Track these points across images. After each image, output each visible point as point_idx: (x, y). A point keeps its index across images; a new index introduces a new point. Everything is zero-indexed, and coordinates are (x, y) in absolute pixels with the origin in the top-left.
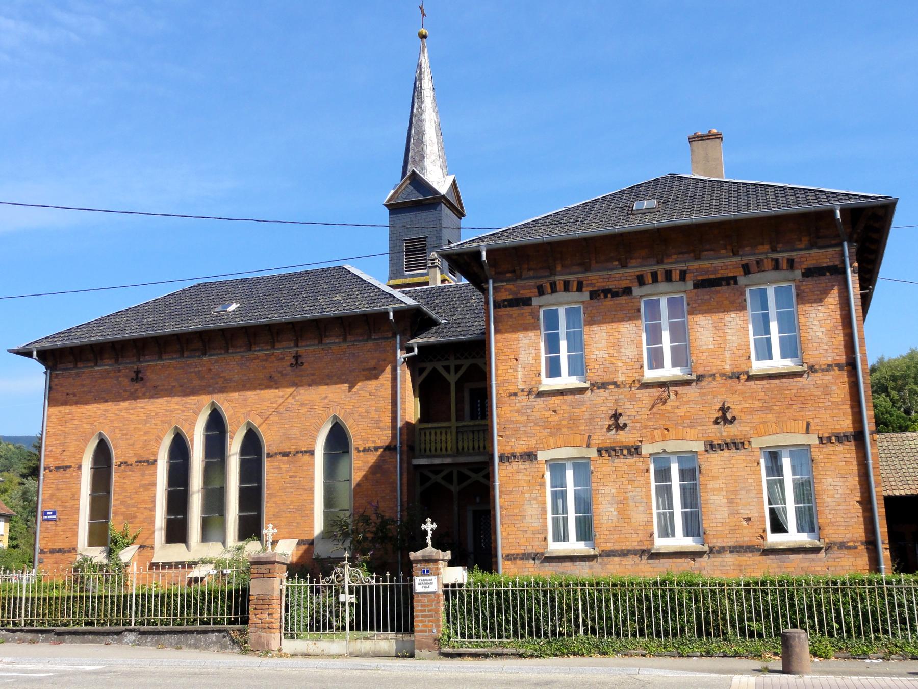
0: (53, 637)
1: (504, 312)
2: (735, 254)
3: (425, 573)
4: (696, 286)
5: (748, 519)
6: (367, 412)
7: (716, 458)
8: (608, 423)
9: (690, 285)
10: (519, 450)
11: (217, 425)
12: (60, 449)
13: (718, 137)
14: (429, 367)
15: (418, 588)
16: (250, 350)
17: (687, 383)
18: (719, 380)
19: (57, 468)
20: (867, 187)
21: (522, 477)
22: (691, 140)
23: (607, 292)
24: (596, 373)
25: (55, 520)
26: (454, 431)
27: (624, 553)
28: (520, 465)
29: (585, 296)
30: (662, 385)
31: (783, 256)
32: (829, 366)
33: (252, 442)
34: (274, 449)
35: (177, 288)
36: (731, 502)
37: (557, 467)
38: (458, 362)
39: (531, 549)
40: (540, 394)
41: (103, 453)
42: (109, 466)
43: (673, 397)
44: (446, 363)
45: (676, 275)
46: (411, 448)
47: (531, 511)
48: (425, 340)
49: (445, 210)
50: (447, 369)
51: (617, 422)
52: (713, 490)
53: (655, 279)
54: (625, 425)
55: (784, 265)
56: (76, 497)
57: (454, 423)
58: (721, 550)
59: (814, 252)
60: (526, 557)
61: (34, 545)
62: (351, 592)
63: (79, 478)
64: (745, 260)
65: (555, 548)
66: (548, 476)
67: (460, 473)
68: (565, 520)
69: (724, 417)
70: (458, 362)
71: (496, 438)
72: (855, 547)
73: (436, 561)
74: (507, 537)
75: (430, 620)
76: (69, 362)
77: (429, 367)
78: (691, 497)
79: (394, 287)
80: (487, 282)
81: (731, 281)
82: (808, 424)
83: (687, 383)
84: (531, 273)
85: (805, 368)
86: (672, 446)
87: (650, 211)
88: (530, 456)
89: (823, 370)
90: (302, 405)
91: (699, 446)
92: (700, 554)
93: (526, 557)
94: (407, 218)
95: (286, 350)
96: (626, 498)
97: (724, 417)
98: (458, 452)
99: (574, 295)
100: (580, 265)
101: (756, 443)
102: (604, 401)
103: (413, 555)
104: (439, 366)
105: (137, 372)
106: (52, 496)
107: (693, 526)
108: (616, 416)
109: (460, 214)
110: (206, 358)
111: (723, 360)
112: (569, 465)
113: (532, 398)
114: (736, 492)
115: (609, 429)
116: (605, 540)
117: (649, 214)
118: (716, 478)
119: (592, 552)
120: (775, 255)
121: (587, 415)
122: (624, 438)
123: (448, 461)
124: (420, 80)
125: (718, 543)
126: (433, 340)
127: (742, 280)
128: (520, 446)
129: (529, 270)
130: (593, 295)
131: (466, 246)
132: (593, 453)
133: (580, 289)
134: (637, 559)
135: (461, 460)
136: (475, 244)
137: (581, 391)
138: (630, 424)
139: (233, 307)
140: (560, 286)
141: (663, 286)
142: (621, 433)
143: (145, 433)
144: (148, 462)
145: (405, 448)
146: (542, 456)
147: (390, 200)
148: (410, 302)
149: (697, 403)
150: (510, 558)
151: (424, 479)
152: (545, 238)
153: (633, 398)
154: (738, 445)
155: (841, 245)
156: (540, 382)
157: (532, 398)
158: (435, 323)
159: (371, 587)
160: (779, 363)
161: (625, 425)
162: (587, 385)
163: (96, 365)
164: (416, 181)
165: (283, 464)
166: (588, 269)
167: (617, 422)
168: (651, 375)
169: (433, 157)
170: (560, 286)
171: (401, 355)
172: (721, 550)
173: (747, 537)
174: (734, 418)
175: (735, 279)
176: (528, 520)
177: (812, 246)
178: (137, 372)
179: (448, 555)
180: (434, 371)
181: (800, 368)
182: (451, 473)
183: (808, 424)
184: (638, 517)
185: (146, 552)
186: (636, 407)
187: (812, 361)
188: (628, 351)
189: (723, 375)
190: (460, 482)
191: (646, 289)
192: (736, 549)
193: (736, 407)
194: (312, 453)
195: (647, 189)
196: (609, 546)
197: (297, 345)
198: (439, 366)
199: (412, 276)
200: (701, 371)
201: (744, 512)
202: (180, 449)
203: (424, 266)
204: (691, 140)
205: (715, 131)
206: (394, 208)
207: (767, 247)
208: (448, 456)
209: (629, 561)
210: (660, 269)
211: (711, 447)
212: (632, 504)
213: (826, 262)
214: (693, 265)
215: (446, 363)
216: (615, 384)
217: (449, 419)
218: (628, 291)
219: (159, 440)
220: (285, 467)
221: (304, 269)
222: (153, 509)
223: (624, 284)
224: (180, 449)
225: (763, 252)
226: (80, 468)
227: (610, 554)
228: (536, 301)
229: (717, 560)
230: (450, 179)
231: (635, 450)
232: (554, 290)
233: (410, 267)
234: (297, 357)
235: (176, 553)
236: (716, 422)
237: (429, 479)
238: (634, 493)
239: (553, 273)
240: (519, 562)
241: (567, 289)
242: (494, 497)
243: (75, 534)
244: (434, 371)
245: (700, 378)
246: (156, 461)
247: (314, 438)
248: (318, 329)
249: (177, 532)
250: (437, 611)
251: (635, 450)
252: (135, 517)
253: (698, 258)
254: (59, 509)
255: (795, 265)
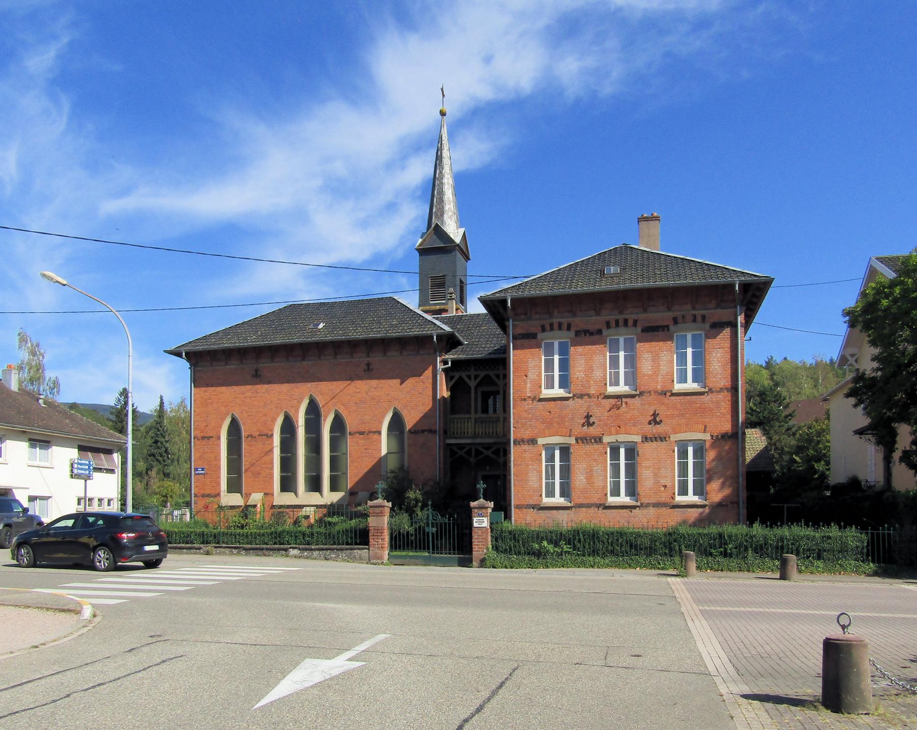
0: (243, 552)
1: (519, 342)
2: (669, 309)
3: (480, 515)
4: (643, 331)
5: (665, 486)
6: (416, 405)
7: (647, 445)
8: (582, 421)
9: (639, 329)
10: (526, 437)
11: (314, 412)
12: (204, 424)
13: (657, 219)
14: (457, 375)
15: (475, 525)
16: (336, 358)
17: (633, 396)
18: (653, 396)
19: (203, 438)
20: (755, 270)
21: (527, 455)
22: (639, 220)
23: (586, 332)
24: (576, 387)
25: (204, 474)
26: (473, 420)
27: (589, 506)
28: (526, 447)
29: (572, 334)
30: (618, 397)
31: (699, 313)
32: (721, 389)
33: (338, 425)
34: (354, 429)
35: (276, 308)
36: (655, 475)
37: (550, 449)
38: (476, 373)
39: (532, 502)
40: (541, 400)
41: (235, 429)
42: (240, 438)
43: (624, 405)
44: (468, 373)
45: (630, 322)
46: (445, 432)
47: (532, 477)
48: (455, 356)
49: (459, 255)
50: (469, 377)
51: (588, 421)
52: (645, 467)
53: (617, 325)
54: (594, 423)
55: (699, 319)
56: (218, 459)
57: (473, 415)
58: (648, 505)
59: (719, 311)
60: (528, 506)
61: (191, 490)
62: (433, 527)
63: (219, 445)
64: (675, 314)
65: (547, 501)
66: (544, 452)
67: (477, 450)
68: (553, 484)
69: (655, 420)
70: (476, 373)
71: (512, 429)
72: (727, 505)
73: (487, 508)
74: (516, 496)
75: (482, 545)
76: (208, 361)
77: (457, 375)
78: (631, 471)
79: (426, 312)
80: (508, 320)
81: (665, 328)
82: (705, 427)
83: (633, 396)
84: (537, 316)
85: (707, 390)
86: (622, 438)
87: (615, 275)
88: (533, 441)
89: (717, 392)
90: (372, 399)
91: (637, 439)
92: (634, 507)
93: (528, 506)
94: (433, 258)
95: (361, 359)
96: (591, 471)
97: (655, 420)
98: (475, 436)
99: (564, 333)
100: (570, 311)
101: (674, 438)
102: (579, 407)
103: (473, 504)
104: (464, 375)
105: (256, 371)
106: (200, 458)
107: (632, 491)
108: (588, 417)
109: (467, 258)
110: (304, 363)
111: (657, 382)
112: (558, 447)
113: (535, 403)
114: (659, 469)
115: (583, 425)
116: (577, 497)
117: (616, 279)
118: (647, 459)
119: (569, 504)
120: (694, 312)
121: (570, 416)
122: (593, 431)
123: (469, 441)
124: (441, 150)
125: (646, 501)
126: (461, 356)
127: (672, 328)
128: (527, 434)
129: (536, 313)
130: (577, 333)
131: (497, 295)
132: (572, 441)
133: (569, 329)
134: (596, 509)
135: (478, 441)
136: (503, 295)
137: (567, 399)
138: (597, 423)
139: (321, 326)
140: (556, 326)
141: (622, 329)
142: (591, 428)
143: (264, 415)
144: (266, 435)
145: (442, 432)
146: (541, 441)
147: (420, 245)
148: (447, 328)
149: (639, 409)
150: (518, 507)
151: (453, 453)
152: (550, 292)
153: (599, 405)
154: (662, 438)
155: (736, 307)
156: (541, 392)
157: (535, 403)
158: (459, 343)
159: (445, 524)
160: (691, 385)
161: (594, 423)
162: (571, 395)
163: (227, 364)
164: (439, 232)
165: (361, 440)
166: (574, 315)
167: (588, 421)
168: (611, 390)
169: (450, 214)
170: (556, 326)
171: (440, 366)
172: (648, 505)
173: (664, 497)
174: (661, 421)
175: (668, 326)
176: (531, 483)
177: (718, 306)
178: (256, 371)
179: (491, 505)
180: (460, 378)
181: (703, 390)
182: (471, 449)
183: (705, 427)
184: (598, 483)
185: (269, 498)
186: (600, 412)
187: (711, 385)
188: (598, 374)
189: (656, 392)
190: (476, 456)
191: (611, 331)
192: (657, 505)
193: (663, 412)
194: (380, 433)
195: (610, 256)
196: (580, 501)
197: (368, 356)
198: (464, 375)
199: (436, 304)
200: (643, 389)
201: (663, 482)
202: (289, 428)
203: (444, 298)
204: (639, 220)
205: (655, 214)
206: (423, 252)
207: (689, 306)
208: (469, 438)
209: (592, 510)
210: (621, 317)
211: (646, 439)
212: (595, 475)
213: (725, 319)
214: (642, 316)
215: (468, 373)
216: (589, 395)
217: (469, 412)
218: (600, 332)
219: (274, 420)
220: (362, 442)
221: (365, 298)
222: (272, 468)
223: (597, 327)
224: (289, 428)
225: (686, 310)
226: (219, 438)
227: (580, 506)
228: (540, 336)
229: (645, 511)
230: (462, 231)
231: (599, 440)
232: (552, 329)
233: (434, 299)
234: (368, 365)
235: (288, 499)
236: (650, 423)
237: (456, 453)
238: (597, 468)
239: (551, 315)
240: (524, 510)
241: (560, 328)
242: (510, 467)
243: (219, 484)
244: (460, 378)
245: (641, 394)
246: (272, 435)
247: (381, 423)
248: (384, 344)
249: (288, 484)
250: (487, 540)
251: (599, 440)
252: (259, 474)
253: (645, 311)
254: (206, 467)
255: (706, 320)
